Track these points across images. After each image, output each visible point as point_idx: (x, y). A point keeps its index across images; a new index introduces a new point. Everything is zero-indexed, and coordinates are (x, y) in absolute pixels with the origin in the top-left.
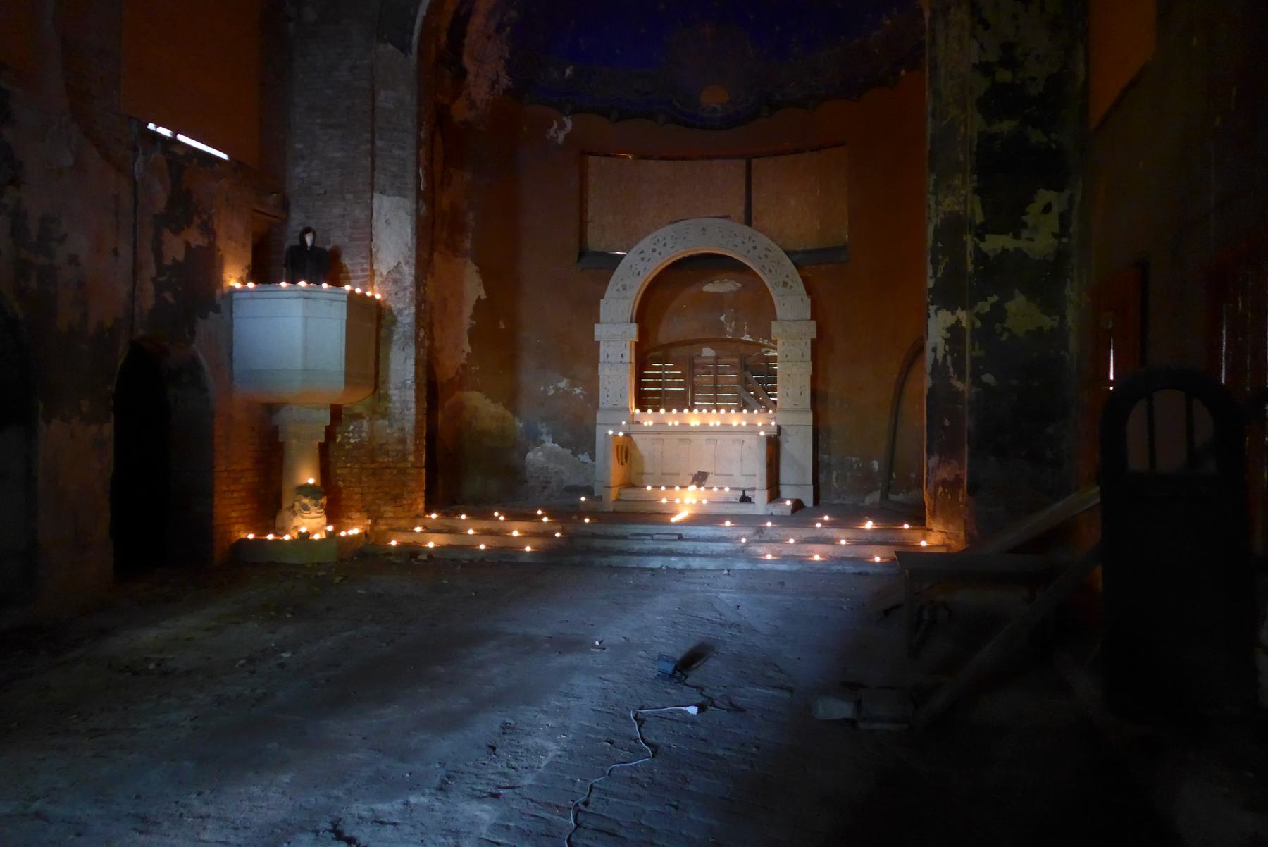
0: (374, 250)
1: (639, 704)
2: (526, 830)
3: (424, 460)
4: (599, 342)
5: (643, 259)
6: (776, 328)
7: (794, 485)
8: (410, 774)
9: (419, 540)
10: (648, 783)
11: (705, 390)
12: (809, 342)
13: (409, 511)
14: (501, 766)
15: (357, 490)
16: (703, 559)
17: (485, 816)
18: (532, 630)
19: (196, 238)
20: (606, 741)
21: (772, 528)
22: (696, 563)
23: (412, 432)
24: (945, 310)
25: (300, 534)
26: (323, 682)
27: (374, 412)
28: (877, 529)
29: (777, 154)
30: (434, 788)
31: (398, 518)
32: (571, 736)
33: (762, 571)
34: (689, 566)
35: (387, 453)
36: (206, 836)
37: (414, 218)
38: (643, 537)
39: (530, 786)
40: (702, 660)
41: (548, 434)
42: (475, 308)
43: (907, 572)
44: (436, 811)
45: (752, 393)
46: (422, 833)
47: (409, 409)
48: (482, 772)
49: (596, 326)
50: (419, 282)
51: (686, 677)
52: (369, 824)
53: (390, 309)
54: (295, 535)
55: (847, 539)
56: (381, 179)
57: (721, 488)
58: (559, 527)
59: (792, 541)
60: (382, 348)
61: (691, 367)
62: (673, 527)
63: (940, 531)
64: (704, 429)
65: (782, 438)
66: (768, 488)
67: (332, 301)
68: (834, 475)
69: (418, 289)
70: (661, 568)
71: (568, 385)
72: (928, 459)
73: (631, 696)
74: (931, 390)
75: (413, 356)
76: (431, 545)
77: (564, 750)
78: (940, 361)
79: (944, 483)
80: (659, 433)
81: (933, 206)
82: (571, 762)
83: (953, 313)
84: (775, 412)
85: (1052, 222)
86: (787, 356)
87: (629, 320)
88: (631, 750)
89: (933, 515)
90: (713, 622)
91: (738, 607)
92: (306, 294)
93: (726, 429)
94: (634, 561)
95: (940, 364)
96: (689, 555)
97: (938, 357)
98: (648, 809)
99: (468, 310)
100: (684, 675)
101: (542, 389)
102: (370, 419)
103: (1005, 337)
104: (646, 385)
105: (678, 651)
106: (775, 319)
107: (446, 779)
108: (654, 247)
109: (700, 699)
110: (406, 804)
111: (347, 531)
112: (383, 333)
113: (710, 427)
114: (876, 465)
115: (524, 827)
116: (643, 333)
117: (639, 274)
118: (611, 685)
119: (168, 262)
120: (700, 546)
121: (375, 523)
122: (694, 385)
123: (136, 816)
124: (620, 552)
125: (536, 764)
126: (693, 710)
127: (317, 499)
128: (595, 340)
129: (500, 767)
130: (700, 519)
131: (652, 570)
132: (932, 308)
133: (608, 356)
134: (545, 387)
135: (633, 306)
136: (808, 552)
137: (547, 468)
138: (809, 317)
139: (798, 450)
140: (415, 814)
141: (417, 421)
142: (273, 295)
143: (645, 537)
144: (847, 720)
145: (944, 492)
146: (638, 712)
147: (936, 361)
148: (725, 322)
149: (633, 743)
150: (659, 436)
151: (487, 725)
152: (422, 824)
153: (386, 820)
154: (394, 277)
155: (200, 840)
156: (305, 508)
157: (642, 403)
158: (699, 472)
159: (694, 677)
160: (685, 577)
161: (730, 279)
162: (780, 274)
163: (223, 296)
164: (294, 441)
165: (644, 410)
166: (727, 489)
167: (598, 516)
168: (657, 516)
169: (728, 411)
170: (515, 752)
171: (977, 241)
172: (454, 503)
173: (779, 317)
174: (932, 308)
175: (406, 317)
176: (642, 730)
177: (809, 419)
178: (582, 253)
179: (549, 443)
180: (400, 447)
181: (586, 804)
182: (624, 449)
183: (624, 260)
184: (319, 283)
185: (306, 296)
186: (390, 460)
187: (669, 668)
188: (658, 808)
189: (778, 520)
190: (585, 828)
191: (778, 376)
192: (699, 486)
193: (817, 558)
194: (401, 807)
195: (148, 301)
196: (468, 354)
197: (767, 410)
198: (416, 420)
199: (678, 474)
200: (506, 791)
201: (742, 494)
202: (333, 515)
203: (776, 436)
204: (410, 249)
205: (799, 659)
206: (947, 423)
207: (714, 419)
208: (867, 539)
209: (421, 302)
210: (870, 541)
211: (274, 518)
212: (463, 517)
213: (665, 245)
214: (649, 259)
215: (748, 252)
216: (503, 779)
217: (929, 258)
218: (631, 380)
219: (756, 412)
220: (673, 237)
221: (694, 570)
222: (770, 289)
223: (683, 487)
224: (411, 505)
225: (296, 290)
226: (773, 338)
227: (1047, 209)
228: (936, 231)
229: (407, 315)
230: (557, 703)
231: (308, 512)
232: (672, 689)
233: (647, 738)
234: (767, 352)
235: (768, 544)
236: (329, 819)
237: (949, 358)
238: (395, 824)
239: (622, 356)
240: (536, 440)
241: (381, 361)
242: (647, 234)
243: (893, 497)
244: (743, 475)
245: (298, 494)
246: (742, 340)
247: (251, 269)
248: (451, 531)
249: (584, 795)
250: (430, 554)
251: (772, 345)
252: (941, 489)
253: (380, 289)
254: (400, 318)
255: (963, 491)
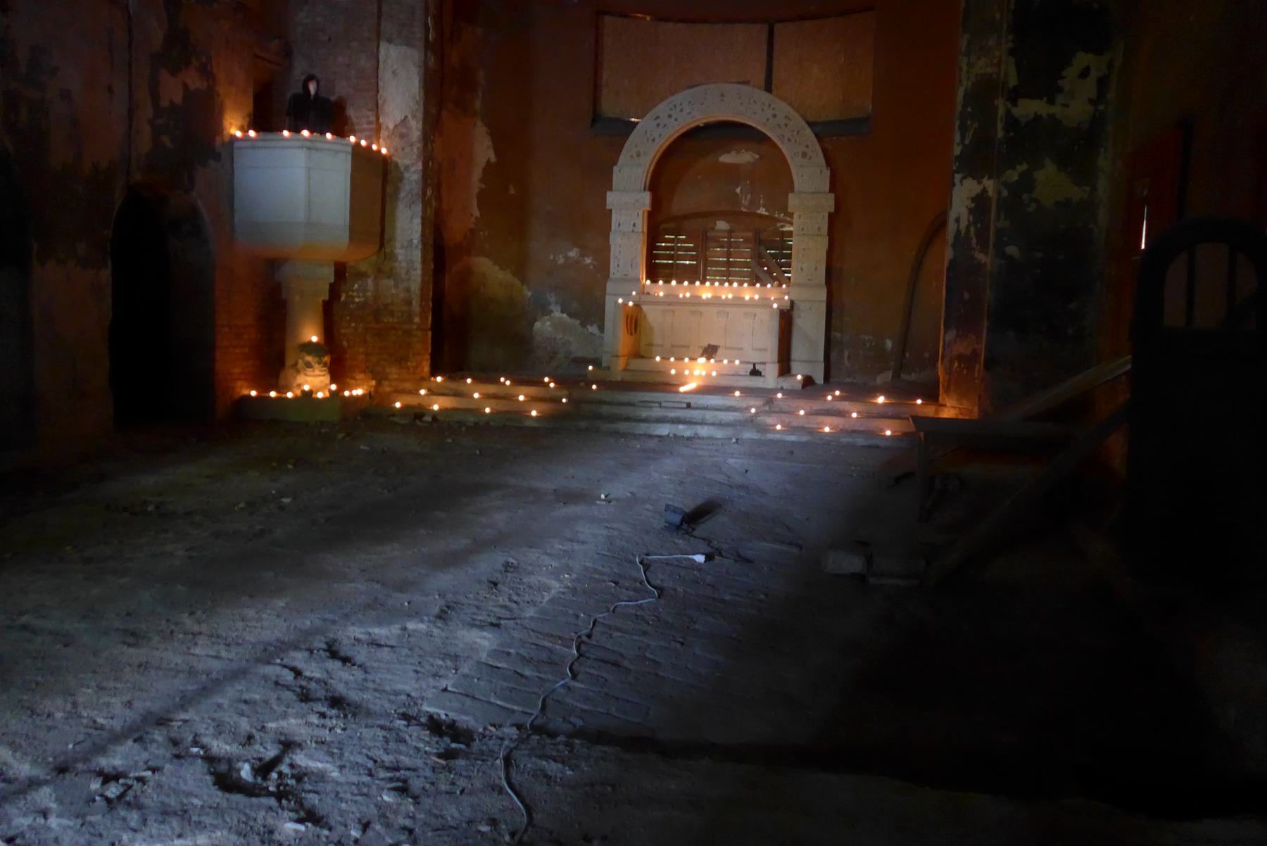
0: (380, 102)
1: (646, 551)
2: (527, 657)
3: (430, 322)
4: (611, 210)
5: (658, 125)
6: (793, 201)
7: (805, 361)
8: (409, 603)
9: (424, 403)
10: (653, 620)
11: (718, 264)
12: (827, 215)
13: (414, 373)
14: (502, 600)
15: (361, 350)
16: (712, 427)
17: (486, 643)
18: (537, 484)
19: (195, 81)
20: (610, 581)
21: (781, 399)
22: (704, 431)
23: (417, 292)
24: (971, 178)
25: (303, 392)
26: (322, 521)
27: (380, 271)
28: (889, 403)
29: (802, 18)
30: (433, 616)
31: (402, 381)
32: (574, 576)
33: (772, 441)
34: (696, 434)
35: (392, 314)
36: (197, 651)
37: (422, 70)
38: (650, 405)
39: (531, 618)
40: (710, 516)
41: (556, 303)
42: (485, 170)
43: (922, 434)
44: (434, 637)
45: (766, 268)
46: (419, 656)
47: (415, 270)
48: (482, 604)
49: (609, 193)
50: (426, 138)
51: (693, 530)
52: (366, 646)
53: (397, 165)
54: (298, 393)
55: (858, 413)
56: (387, 26)
57: (731, 362)
58: (565, 392)
59: (802, 412)
60: (388, 207)
61: (703, 241)
62: (681, 395)
63: (954, 407)
64: (716, 302)
65: (795, 314)
66: (779, 362)
67: (337, 152)
68: (846, 354)
69: (425, 145)
70: (668, 436)
71: (578, 255)
72: (945, 332)
73: (638, 544)
74: (952, 262)
75: (420, 214)
76: (436, 407)
77: (568, 588)
78: (963, 232)
79: (960, 358)
80: (670, 304)
81: (965, 67)
82: (574, 599)
83: (980, 183)
84: (788, 286)
85: (1091, 82)
86: (803, 229)
87: (643, 188)
88: (635, 590)
89: (947, 390)
90: (720, 483)
91: (746, 471)
92: (309, 144)
93: (738, 302)
94: (642, 428)
95: (963, 235)
96: (696, 423)
97: (960, 228)
98: (653, 644)
99: (477, 174)
100: (691, 527)
101: (552, 257)
102: (375, 278)
103: (1034, 206)
104: (658, 257)
105: (689, 505)
106: (793, 191)
107: (446, 609)
108: (670, 112)
109: (708, 550)
110: (405, 629)
111: (351, 391)
112: (389, 190)
113: (722, 300)
114: (889, 344)
115: (525, 654)
116: (657, 204)
117: (654, 140)
118: (616, 533)
119: (165, 103)
120: (709, 415)
121: (379, 384)
122: (707, 260)
123: (125, 631)
124: (628, 419)
125: (539, 599)
126: (700, 558)
127: (320, 357)
128: (607, 208)
129: (501, 600)
130: (708, 389)
131: (660, 437)
132: (958, 177)
133: (619, 224)
134: (554, 257)
135: (650, 165)
136: (818, 423)
137: (555, 338)
138: (828, 191)
139: (810, 326)
140: (412, 639)
141: (423, 235)
142: (273, 144)
143: (653, 405)
144: (853, 575)
145: (959, 366)
146: (643, 558)
147: (958, 231)
148: (740, 195)
149: (638, 584)
150: (670, 307)
151: (490, 563)
152: (420, 648)
153: (383, 643)
154: (401, 131)
155: (190, 654)
156: (309, 365)
157: (653, 274)
158: (709, 345)
159: (702, 529)
160: (692, 444)
161: (747, 150)
162: (800, 144)
163: (223, 144)
164: (297, 298)
165: (654, 281)
166: (737, 362)
167: (605, 384)
168: (668, 386)
169: (741, 284)
170: (516, 588)
171: (1010, 106)
172: (461, 369)
173: (796, 189)
174: (958, 177)
175: (413, 175)
176: (647, 573)
177: (822, 295)
178: (596, 118)
179: (557, 313)
180: (405, 308)
181: (589, 636)
182: (634, 321)
183: (638, 127)
184: (323, 133)
185: (309, 147)
186: (396, 320)
187: (677, 519)
188: (662, 643)
189: (789, 393)
190: (588, 658)
191: (794, 252)
192: (708, 359)
193: (827, 430)
194: (399, 632)
195: (144, 143)
196: (476, 218)
197: (780, 285)
198: (422, 281)
199: (688, 347)
200: (506, 621)
201: (752, 367)
202: (338, 373)
203: (788, 311)
204: (417, 102)
205: (808, 519)
206: (966, 296)
207: (727, 292)
208: (878, 413)
209: (428, 158)
210: (882, 414)
211: (277, 376)
212: (469, 381)
213: (682, 110)
214: (665, 125)
215: (768, 120)
216: (503, 611)
217: (957, 123)
218: (642, 250)
219: (769, 286)
220: (690, 102)
221: (700, 438)
222: (789, 161)
223: (693, 359)
224: (416, 367)
225: (298, 140)
226: (790, 210)
227: (1085, 73)
228: (966, 95)
229: (414, 172)
230: (560, 547)
231: (311, 369)
232: (678, 539)
233: (653, 582)
234: (782, 227)
235: (777, 415)
236: (323, 639)
237: (972, 229)
238: (392, 647)
239: (634, 225)
240: (545, 311)
241: (387, 219)
242: (662, 100)
243: (904, 377)
244: (756, 350)
245: (302, 351)
246: (758, 214)
247: (252, 117)
248: (456, 394)
249: (587, 628)
250: (435, 416)
251: (788, 219)
252: (956, 364)
253: (386, 144)
254: (406, 175)
255: (979, 368)
